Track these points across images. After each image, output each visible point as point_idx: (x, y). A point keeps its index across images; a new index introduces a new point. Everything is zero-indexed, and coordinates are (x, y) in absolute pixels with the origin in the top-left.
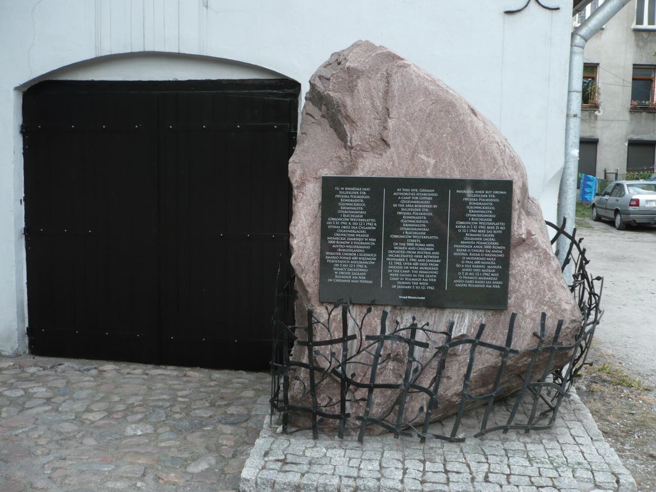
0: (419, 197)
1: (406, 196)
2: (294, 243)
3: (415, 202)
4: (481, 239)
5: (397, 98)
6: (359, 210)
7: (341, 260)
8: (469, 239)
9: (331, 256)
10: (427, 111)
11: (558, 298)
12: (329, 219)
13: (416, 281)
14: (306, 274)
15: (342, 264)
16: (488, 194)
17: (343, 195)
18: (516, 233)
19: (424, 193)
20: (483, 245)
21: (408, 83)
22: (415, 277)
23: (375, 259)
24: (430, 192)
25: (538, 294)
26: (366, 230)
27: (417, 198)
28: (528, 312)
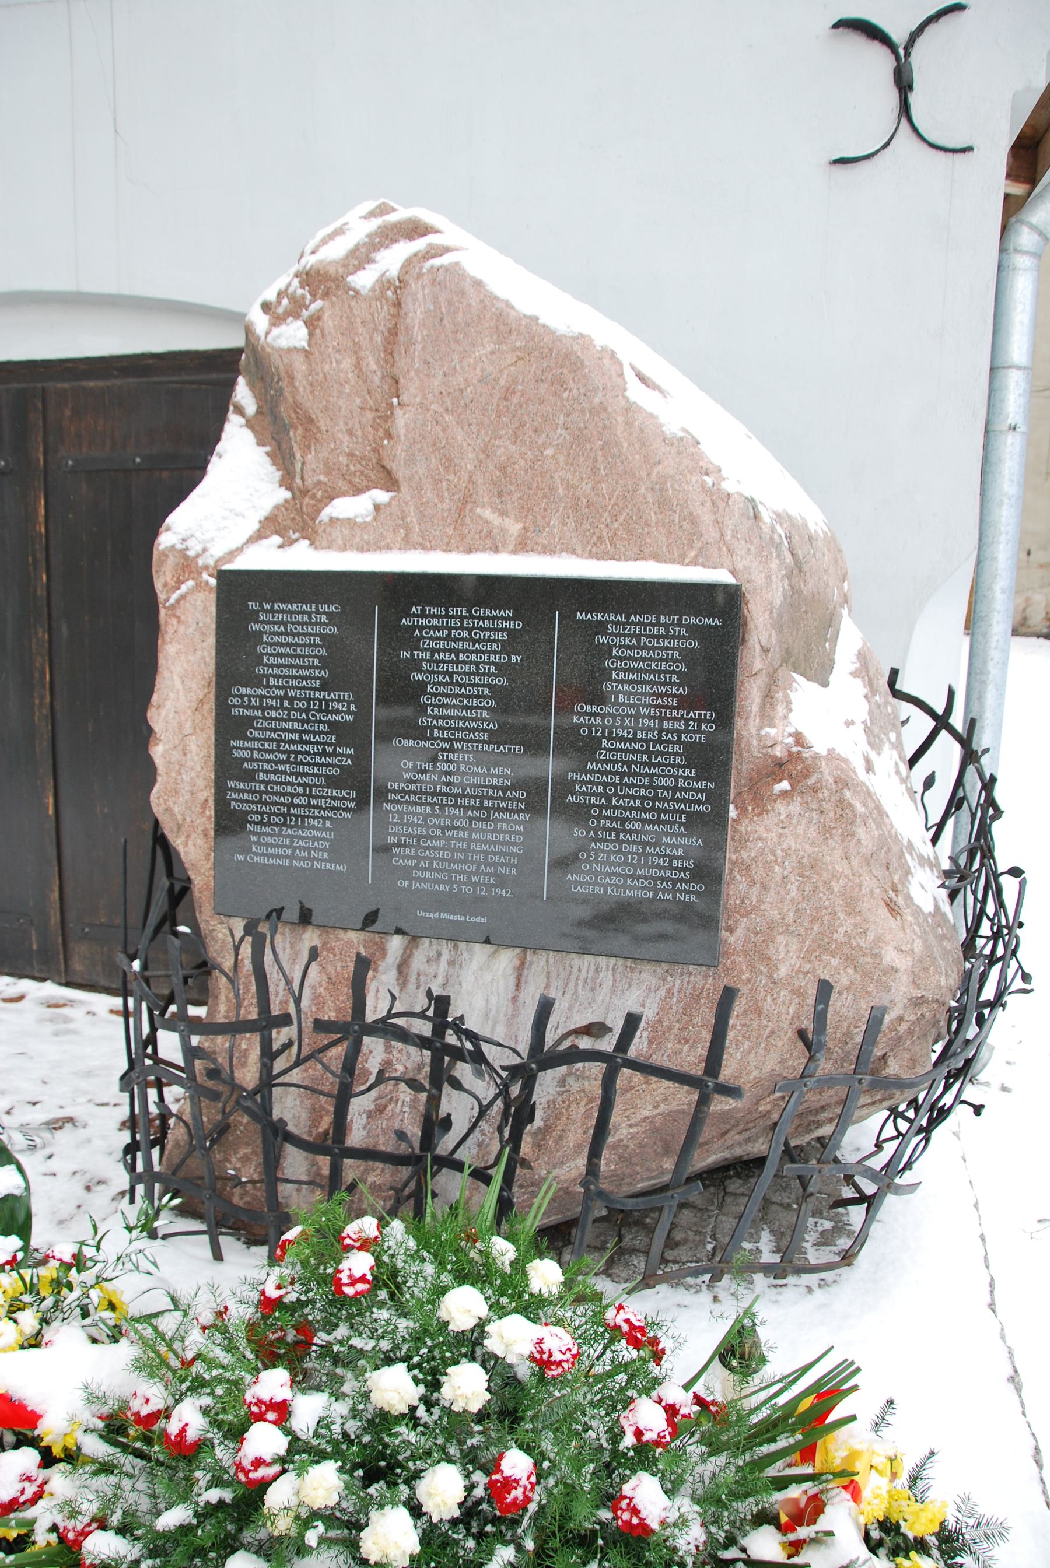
0: (470, 630)
1: (436, 628)
2: (157, 752)
3: (459, 645)
4: (645, 758)
5: (419, 347)
6: (308, 667)
7: (266, 803)
8: (609, 756)
9: (240, 791)
10: (502, 382)
11: (871, 936)
12: (234, 691)
13: (464, 872)
14: (188, 836)
15: (270, 814)
16: (666, 625)
17: (269, 622)
18: (755, 742)
19: (483, 619)
20: (651, 776)
21: (450, 303)
22: (461, 861)
23: (352, 805)
24: (503, 618)
25: (814, 920)
26: (329, 722)
27: (466, 634)
28: (783, 971)
